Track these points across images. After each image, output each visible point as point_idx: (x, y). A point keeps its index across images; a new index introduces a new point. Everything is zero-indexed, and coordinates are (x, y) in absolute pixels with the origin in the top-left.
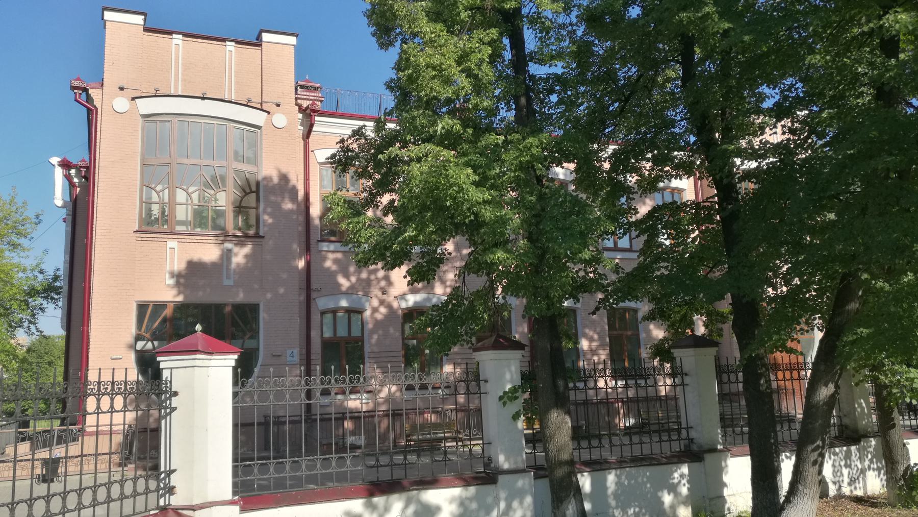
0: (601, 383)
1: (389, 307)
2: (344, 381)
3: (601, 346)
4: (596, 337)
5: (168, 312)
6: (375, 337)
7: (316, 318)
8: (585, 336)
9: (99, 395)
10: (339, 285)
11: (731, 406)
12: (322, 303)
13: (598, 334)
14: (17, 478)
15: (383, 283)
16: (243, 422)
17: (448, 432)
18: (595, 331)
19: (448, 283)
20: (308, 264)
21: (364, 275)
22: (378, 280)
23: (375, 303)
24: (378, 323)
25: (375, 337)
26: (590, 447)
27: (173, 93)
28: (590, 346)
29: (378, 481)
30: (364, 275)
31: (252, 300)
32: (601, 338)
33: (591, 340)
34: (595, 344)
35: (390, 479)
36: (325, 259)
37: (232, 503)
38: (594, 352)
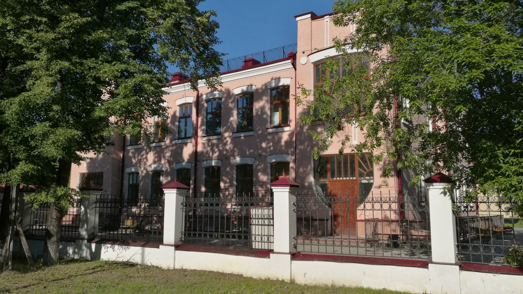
0: (229, 206)
1: (146, 170)
2: (248, 199)
3: (231, 185)
4: (228, 181)
5: (86, 176)
6: (142, 183)
7: (126, 176)
8: (223, 181)
9: (373, 202)
10: (132, 162)
11: (255, 225)
12: (128, 170)
13: (229, 179)
14: (263, 226)
15: (145, 160)
16: (320, 218)
17: (16, 206)
18: (228, 178)
19: (166, 158)
20: (123, 155)
21: (139, 158)
22: (144, 159)
23: (142, 168)
24: (143, 177)
25: (142, 183)
26: (326, 245)
28: (225, 186)
29: (383, 256)
30: (139, 158)
31: (101, 171)
32: (231, 182)
33: (225, 182)
34: (227, 185)
35: (391, 256)
36: (129, 152)
37: (456, 264)
38: (227, 189)
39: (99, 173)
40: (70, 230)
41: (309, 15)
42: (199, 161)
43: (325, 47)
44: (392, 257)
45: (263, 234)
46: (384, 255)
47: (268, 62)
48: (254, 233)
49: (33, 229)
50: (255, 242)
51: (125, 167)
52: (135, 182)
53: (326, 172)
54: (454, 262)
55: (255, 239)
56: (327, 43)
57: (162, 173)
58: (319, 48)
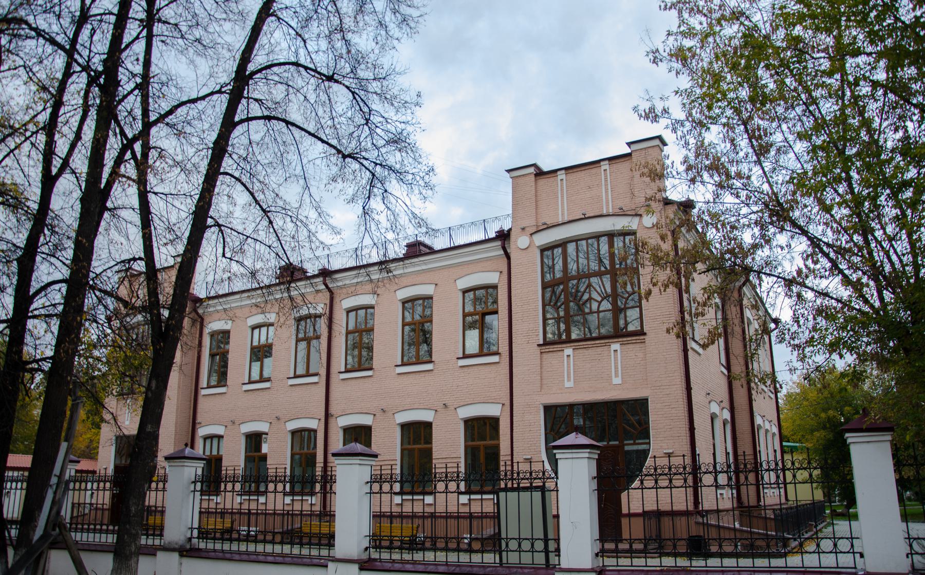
27: (605, 212)
39: (118, 453)
40: (664, 482)
41: (532, 170)
42: (332, 416)
43: (560, 220)
44: (676, 566)
45: (449, 536)
46: (840, 566)
47: (456, 245)
48: (513, 533)
49: (93, 483)
50: (507, 551)
51: (198, 426)
52: (215, 453)
53: (313, 482)
54: (589, 566)
55: (507, 545)
56: (563, 214)
57: (264, 436)
58: (550, 222)
